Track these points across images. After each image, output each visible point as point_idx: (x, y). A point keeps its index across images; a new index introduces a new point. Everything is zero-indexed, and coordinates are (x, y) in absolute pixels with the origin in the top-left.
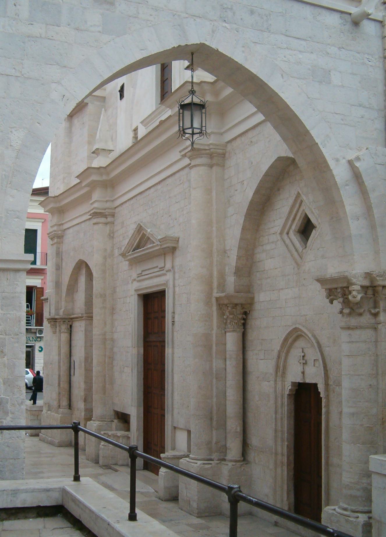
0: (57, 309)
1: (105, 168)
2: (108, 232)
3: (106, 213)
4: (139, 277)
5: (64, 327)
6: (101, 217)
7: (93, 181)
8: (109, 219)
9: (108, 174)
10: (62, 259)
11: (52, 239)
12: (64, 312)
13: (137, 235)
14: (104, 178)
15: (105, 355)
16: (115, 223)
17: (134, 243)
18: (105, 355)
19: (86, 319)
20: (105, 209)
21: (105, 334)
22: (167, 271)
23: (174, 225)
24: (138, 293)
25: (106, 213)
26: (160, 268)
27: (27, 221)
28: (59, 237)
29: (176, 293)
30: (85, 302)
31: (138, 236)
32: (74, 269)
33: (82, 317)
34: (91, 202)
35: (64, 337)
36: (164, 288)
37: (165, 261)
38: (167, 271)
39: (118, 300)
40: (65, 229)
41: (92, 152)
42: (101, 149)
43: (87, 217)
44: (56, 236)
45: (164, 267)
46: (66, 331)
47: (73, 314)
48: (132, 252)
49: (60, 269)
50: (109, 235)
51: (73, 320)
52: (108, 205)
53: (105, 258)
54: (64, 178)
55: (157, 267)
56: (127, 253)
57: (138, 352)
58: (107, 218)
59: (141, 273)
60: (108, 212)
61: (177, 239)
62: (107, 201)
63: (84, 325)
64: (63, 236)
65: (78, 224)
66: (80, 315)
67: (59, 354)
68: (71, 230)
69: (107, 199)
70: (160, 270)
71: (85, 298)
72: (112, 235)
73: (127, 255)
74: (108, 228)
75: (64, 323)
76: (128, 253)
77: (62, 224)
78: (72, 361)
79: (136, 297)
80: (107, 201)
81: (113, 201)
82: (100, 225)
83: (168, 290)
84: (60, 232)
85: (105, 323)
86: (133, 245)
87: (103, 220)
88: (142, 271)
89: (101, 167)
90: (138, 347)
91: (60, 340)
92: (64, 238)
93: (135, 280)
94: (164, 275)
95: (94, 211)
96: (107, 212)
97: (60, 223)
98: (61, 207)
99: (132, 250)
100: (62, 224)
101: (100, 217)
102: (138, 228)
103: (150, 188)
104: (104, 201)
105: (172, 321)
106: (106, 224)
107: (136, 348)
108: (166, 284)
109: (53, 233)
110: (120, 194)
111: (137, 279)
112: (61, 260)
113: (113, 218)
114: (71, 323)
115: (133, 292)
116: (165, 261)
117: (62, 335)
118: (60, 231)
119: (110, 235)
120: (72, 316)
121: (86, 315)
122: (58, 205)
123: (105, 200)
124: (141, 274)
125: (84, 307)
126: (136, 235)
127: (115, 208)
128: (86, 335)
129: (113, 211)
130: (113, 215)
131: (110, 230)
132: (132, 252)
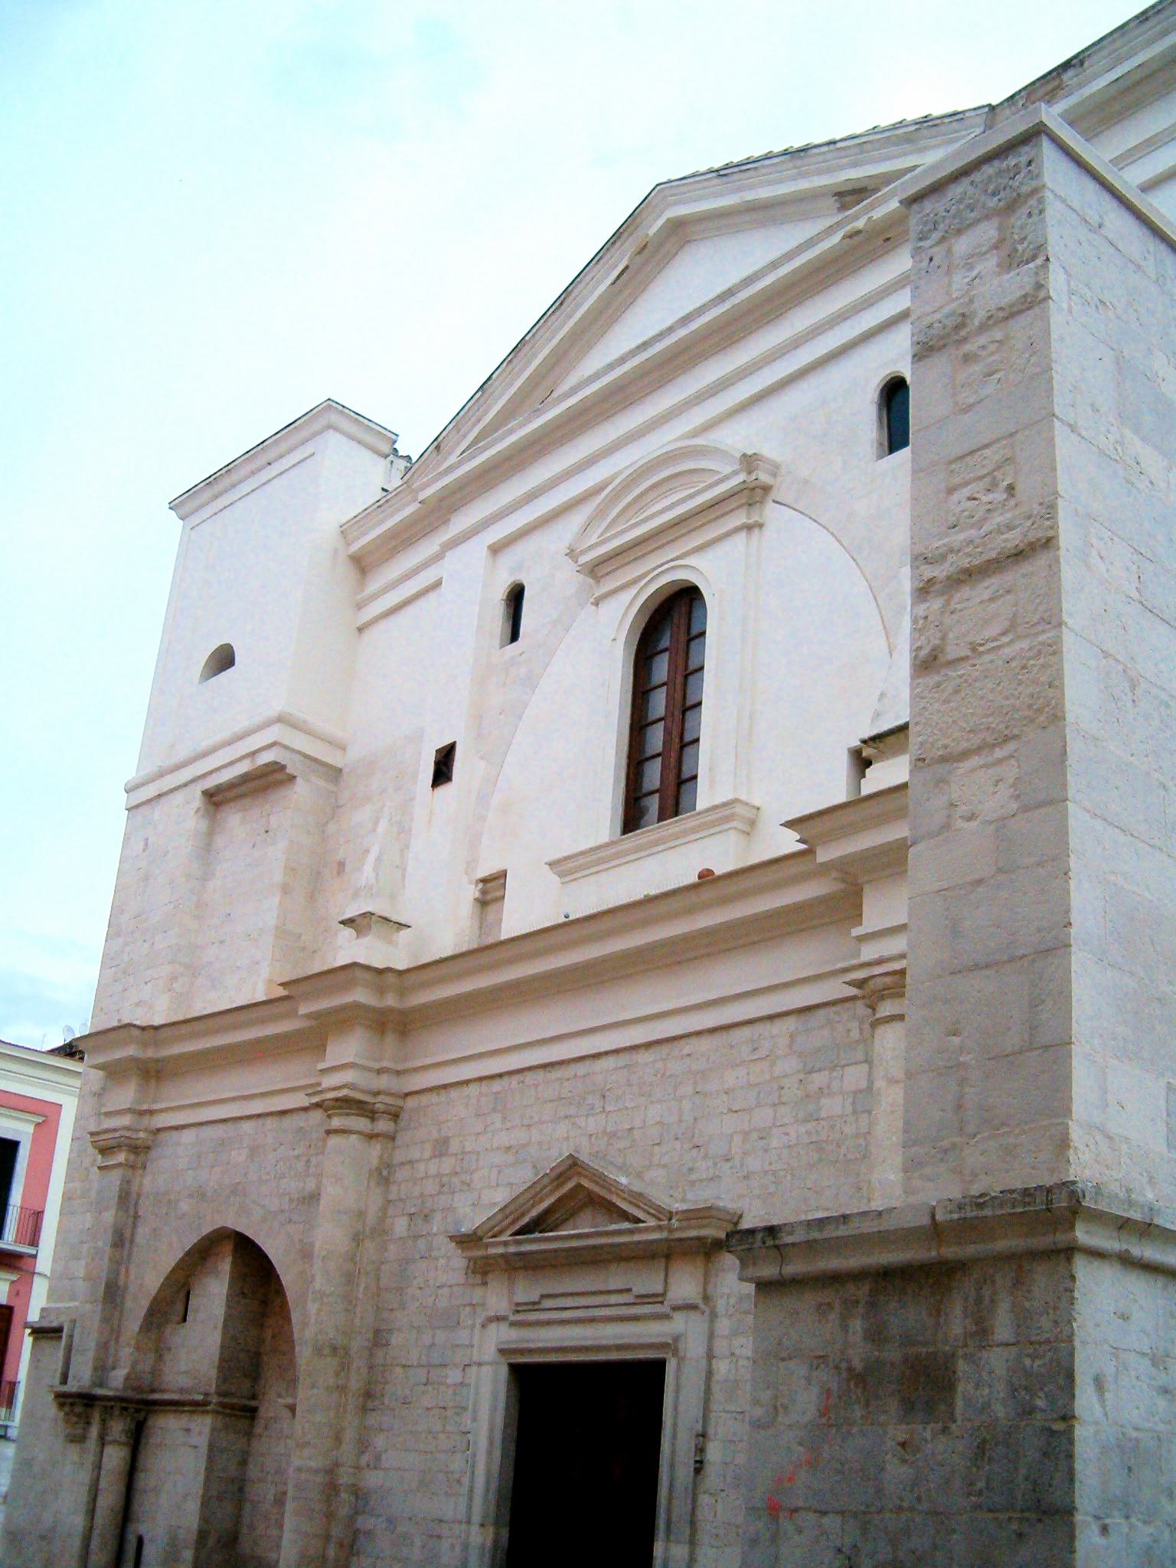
0: (102, 1369)
1: (401, 973)
2: (375, 1162)
3: (377, 1105)
4: (518, 1311)
5: (118, 1428)
6: (358, 1115)
7: (357, 1006)
8: (383, 1125)
9: (402, 993)
10: (136, 1217)
11: (105, 1151)
12: (127, 1378)
13: (548, 1188)
14: (391, 1001)
15: (327, 1538)
16: (399, 1141)
17: (528, 1211)
18: (327, 1538)
19: (218, 1412)
20: (378, 1093)
21: (331, 1471)
22: (676, 1308)
23: (718, 1177)
24: (512, 1361)
25: (377, 1105)
26: (637, 1297)
27: (903, 956)
28: (136, 1148)
29: (717, 1377)
30: (222, 1359)
31: (552, 1192)
32: (188, 1254)
33: (205, 1403)
34: (322, 1066)
35: (115, 1457)
36: (661, 1356)
37: (666, 1276)
38: (676, 1308)
39: (399, 1370)
40: (159, 1130)
41: (340, 919)
42: (380, 917)
43: (300, 1100)
44: (126, 1146)
45: (663, 1295)
46: (123, 1439)
47: (153, 1391)
48: (511, 1235)
49: (127, 1245)
50: (379, 1171)
51: (152, 1408)
52: (384, 1082)
53: (357, 1239)
54: (174, 978)
55: (629, 1290)
56: (490, 1234)
57: (496, 1541)
58: (373, 1119)
59: (537, 1300)
60: (386, 1104)
61: (735, 1220)
62: (380, 1072)
63: (207, 1430)
64: (149, 1148)
65: (259, 1116)
66: (200, 1397)
67: (91, 1512)
68: (188, 1136)
69: (385, 1064)
70: (639, 1301)
71: (222, 1347)
72: (385, 1173)
73: (486, 1240)
74: (375, 1150)
75: (121, 1414)
76: (494, 1236)
77: (151, 1112)
78: (132, 1539)
79: (504, 1371)
80: (380, 1072)
81: (398, 1073)
82: (354, 1136)
83: (678, 1369)
84: (142, 1135)
85: (338, 1439)
86: (523, 1215)
87: (361, 1123)
88: (543, 1297)
89: (389, 970)
90: (497, 1524)
91: (98, 1467)
92: (153, 1154)
93: (499, 1319)
94: (666, 1317)
95: (345, 1096)
96: (380, 1103)
97: (145, 1107)
98: (157, 1061)
99: (517, 1227)
100: (151, 1112)
101: (353, 1114)
102: (559, 1171)
103: (596, 1056)
104: (369, 1070)
105: (696, 1462)
106: (371, 1137)
107: (491, 1530)
108: (673, 1345)
109: (117, 1135)
110: (428, 1061)
111: (512, 1318)
112: (131, 1220)
113: (392, 1124)
114: (141, 1416)
115: (490, 1352)
116: (666, 1276)
117: (109, 1450)
118: (146, 1130)
119: (380, 1174)
120: (157, 1396)
121: (221, 1399)
122: (151, 1053)
123: (377, 1066)
124: (538, 1303)
125: (213, 1373)
126: (545, 1187)
127: (407, 1095)
128: (210, 1459)
129: (399, 1102)
130: (395, 1116)
131: (381, 1158)
132: (511, 1235)
